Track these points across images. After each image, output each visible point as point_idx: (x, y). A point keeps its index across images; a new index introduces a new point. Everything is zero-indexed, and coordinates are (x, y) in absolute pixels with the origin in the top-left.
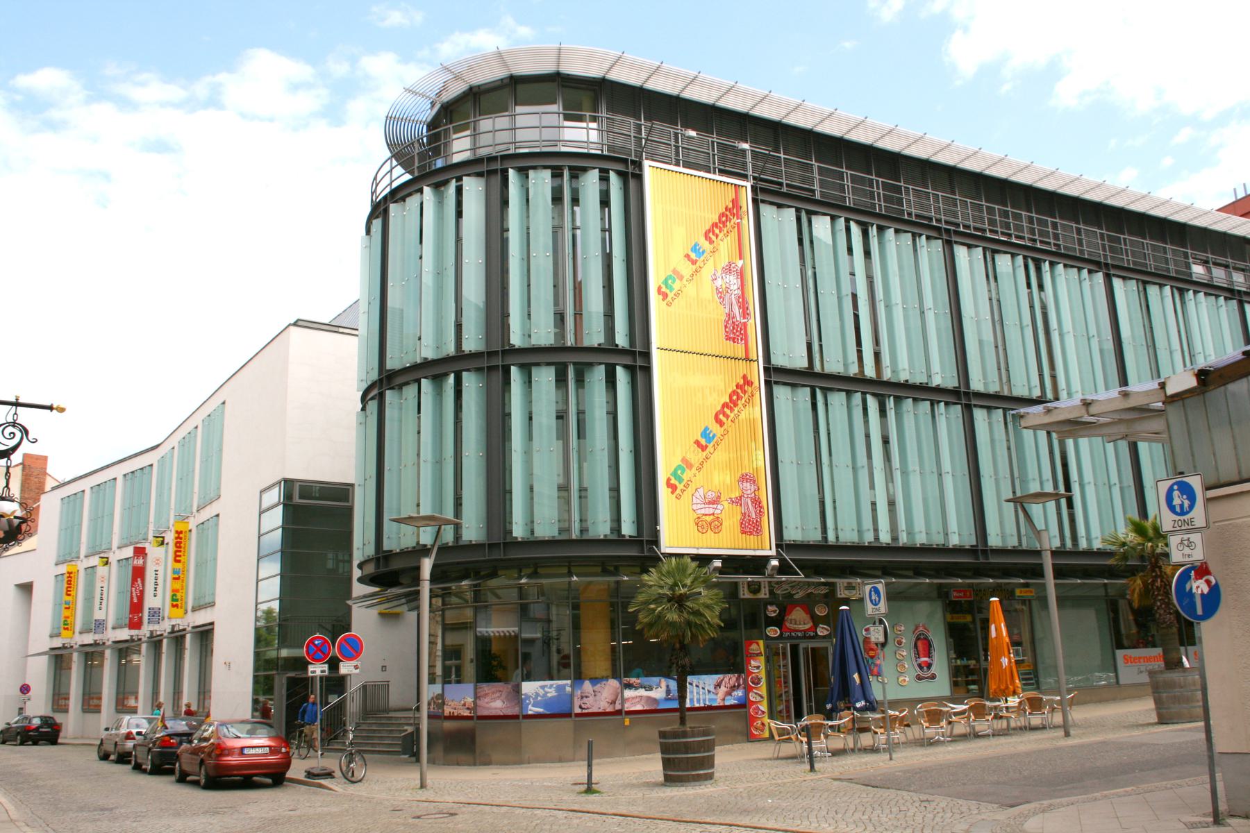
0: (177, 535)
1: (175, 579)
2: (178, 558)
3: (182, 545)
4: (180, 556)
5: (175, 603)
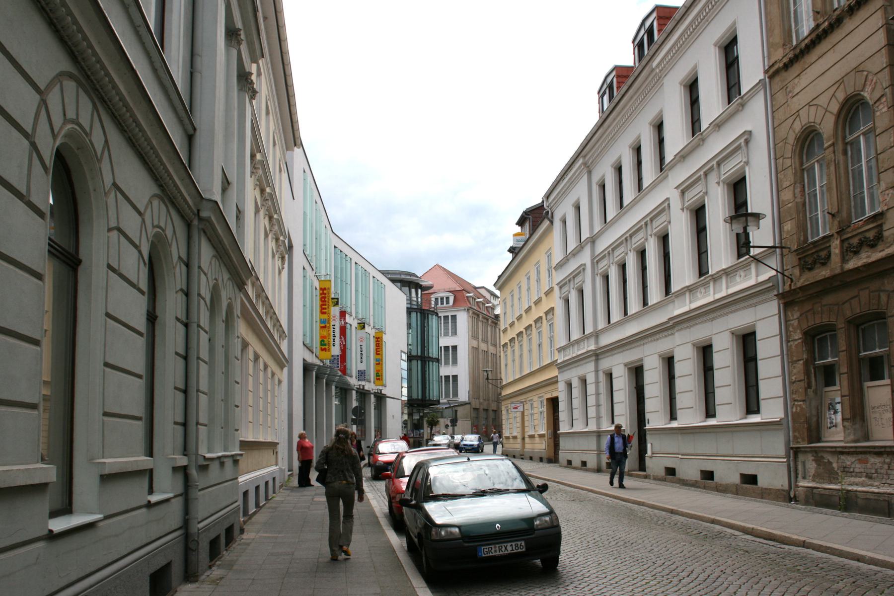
1: (322, 327)
2: (324, 311)
4: (325, 309)
5: (323, 347)
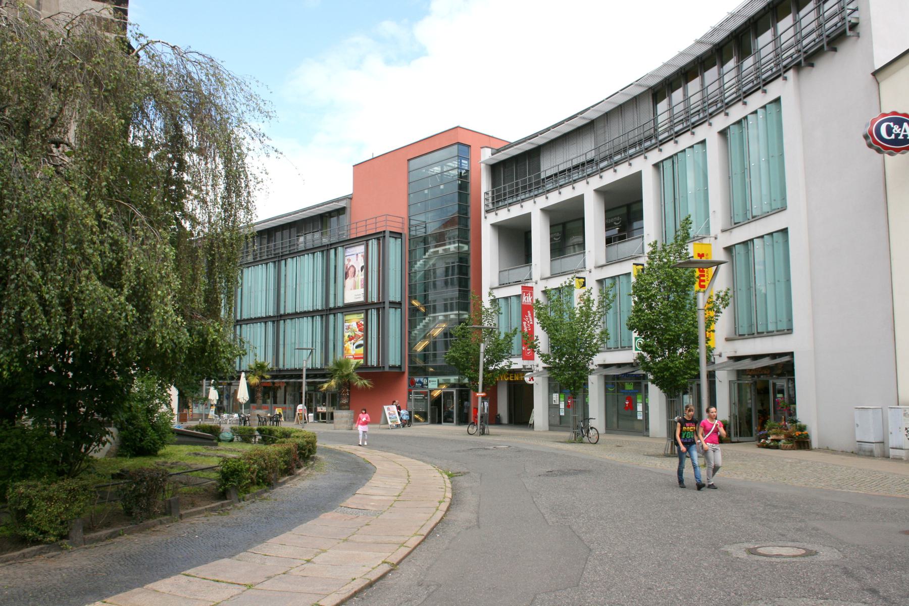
2: (702, 283)
4: (704, 281)
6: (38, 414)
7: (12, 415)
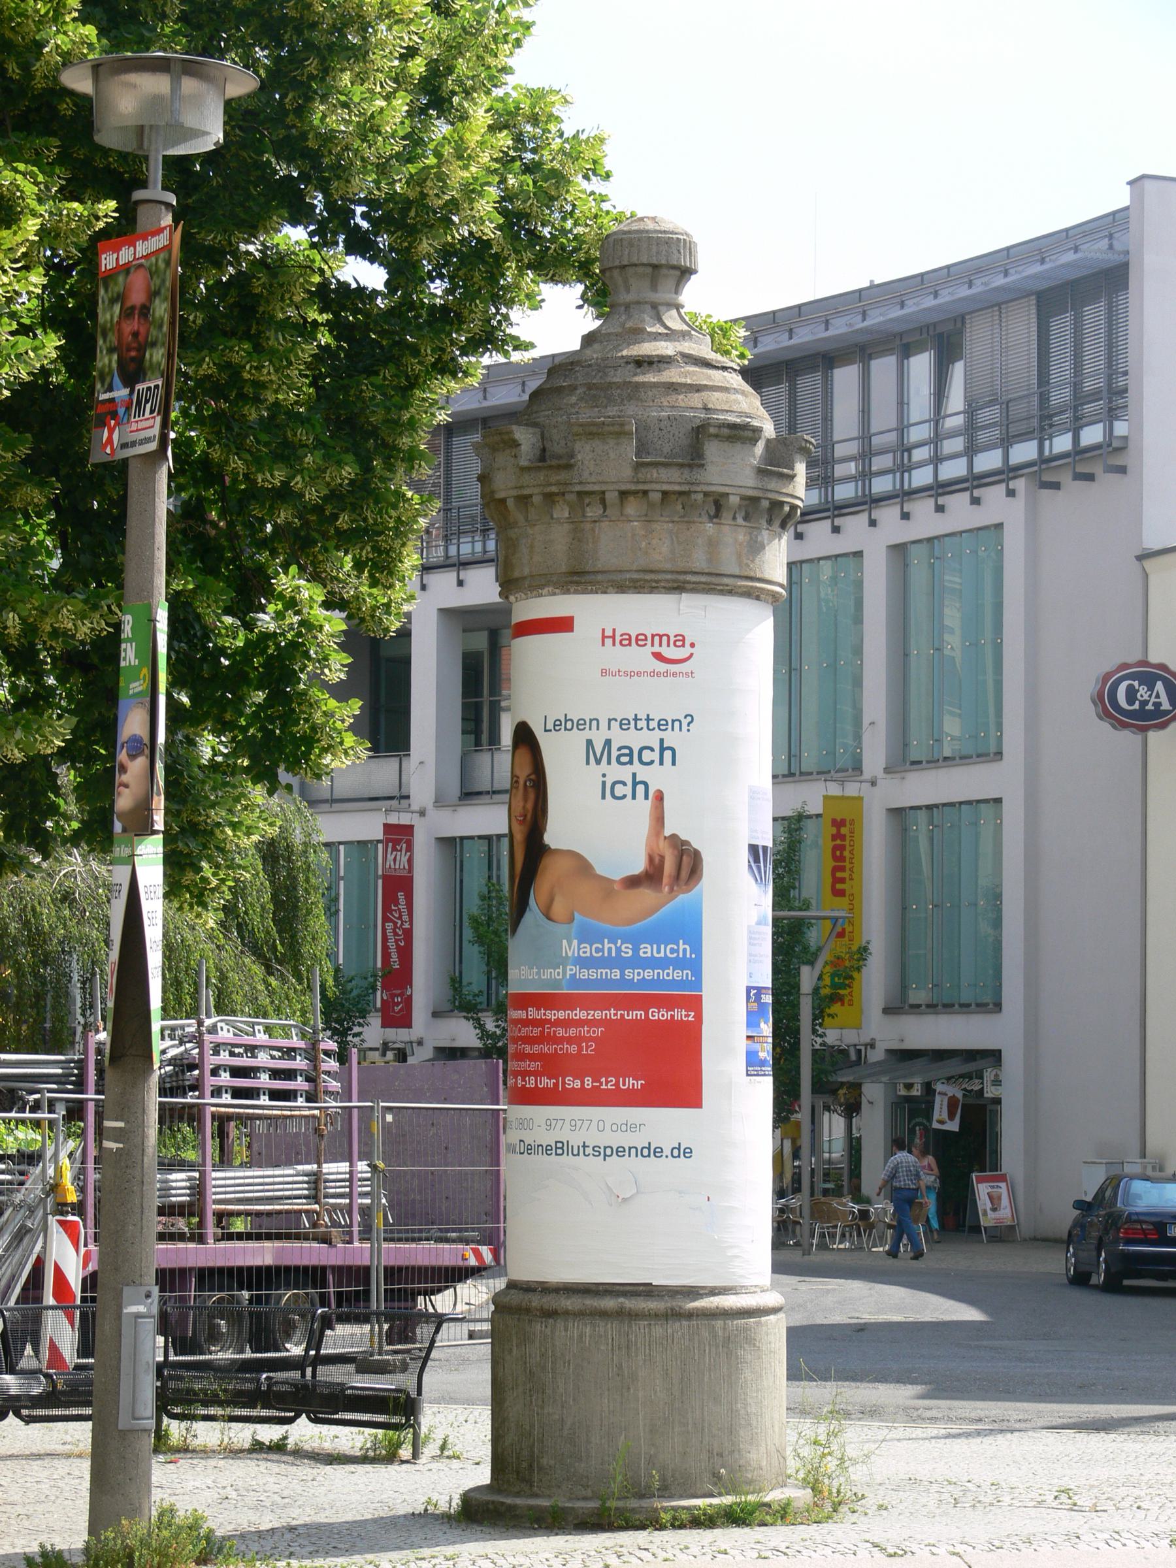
0: (834, 831)
2: (839, 886)
3: (846, 854)
4: (843, 880)
6: (28, 680)
7: (250, 758)
